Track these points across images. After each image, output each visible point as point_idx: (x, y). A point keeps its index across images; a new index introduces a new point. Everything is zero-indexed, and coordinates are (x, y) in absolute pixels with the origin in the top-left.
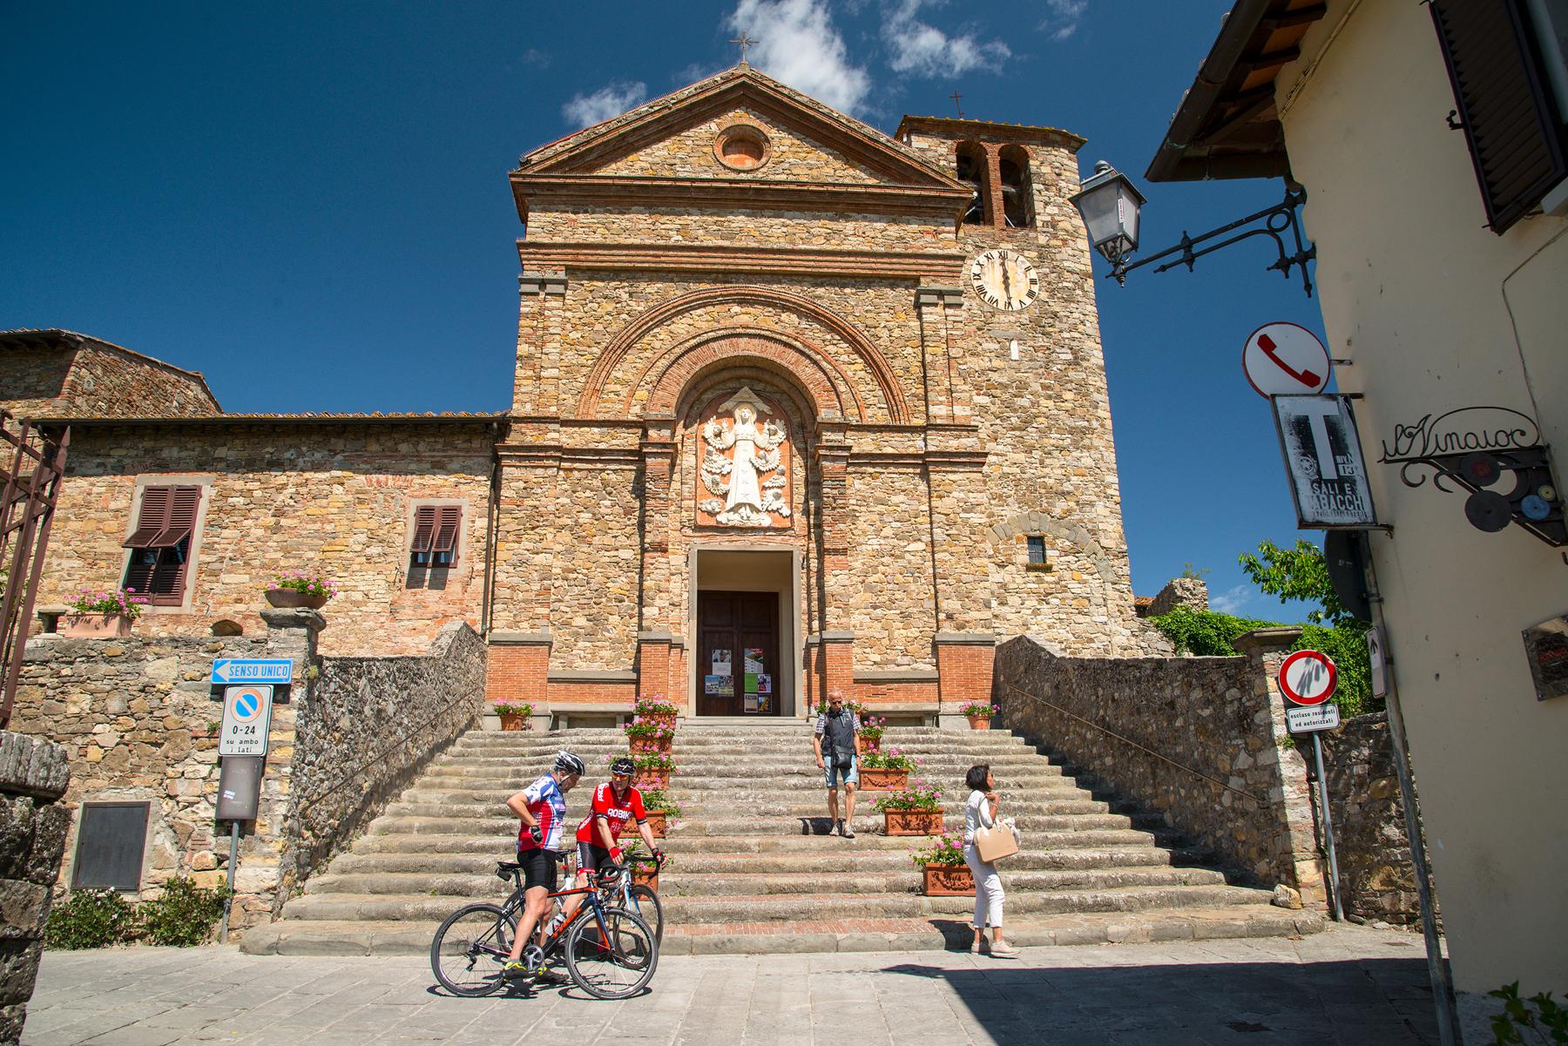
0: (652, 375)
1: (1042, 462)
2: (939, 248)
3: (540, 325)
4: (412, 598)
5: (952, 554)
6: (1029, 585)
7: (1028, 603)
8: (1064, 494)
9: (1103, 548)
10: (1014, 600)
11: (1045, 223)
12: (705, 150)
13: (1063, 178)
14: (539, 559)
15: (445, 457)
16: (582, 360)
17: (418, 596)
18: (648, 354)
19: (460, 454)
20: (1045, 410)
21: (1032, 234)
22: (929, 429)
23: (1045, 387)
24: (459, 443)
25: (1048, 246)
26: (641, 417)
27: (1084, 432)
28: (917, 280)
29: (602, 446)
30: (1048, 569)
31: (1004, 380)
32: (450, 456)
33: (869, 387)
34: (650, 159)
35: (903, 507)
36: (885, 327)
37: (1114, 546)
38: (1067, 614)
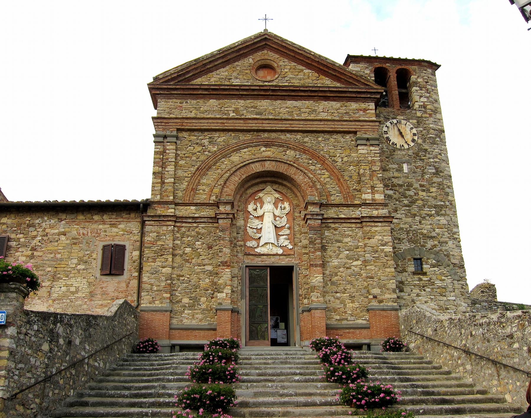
0: (221, 182)
1: (420, 222)
4: (101, 290)
5: (375, 266)
6: (415, 282)
8: (432, 237)
9: (452, 263)
10: (407, 289)
12: (247, 71)
14: (164, 270)
15: (116, 221)
17: (104, 289)
20: (421, 197)
23: (421, 186)
24: (124, 215)
25: (422, 117)
27: (441, 207)
28: (355, 133)
29: (196, 215)
30: (425, 274)
31: (400, 183)
34: (219, 76)
35: (350, 244)
37: (458, 263)
38: (434, 296)
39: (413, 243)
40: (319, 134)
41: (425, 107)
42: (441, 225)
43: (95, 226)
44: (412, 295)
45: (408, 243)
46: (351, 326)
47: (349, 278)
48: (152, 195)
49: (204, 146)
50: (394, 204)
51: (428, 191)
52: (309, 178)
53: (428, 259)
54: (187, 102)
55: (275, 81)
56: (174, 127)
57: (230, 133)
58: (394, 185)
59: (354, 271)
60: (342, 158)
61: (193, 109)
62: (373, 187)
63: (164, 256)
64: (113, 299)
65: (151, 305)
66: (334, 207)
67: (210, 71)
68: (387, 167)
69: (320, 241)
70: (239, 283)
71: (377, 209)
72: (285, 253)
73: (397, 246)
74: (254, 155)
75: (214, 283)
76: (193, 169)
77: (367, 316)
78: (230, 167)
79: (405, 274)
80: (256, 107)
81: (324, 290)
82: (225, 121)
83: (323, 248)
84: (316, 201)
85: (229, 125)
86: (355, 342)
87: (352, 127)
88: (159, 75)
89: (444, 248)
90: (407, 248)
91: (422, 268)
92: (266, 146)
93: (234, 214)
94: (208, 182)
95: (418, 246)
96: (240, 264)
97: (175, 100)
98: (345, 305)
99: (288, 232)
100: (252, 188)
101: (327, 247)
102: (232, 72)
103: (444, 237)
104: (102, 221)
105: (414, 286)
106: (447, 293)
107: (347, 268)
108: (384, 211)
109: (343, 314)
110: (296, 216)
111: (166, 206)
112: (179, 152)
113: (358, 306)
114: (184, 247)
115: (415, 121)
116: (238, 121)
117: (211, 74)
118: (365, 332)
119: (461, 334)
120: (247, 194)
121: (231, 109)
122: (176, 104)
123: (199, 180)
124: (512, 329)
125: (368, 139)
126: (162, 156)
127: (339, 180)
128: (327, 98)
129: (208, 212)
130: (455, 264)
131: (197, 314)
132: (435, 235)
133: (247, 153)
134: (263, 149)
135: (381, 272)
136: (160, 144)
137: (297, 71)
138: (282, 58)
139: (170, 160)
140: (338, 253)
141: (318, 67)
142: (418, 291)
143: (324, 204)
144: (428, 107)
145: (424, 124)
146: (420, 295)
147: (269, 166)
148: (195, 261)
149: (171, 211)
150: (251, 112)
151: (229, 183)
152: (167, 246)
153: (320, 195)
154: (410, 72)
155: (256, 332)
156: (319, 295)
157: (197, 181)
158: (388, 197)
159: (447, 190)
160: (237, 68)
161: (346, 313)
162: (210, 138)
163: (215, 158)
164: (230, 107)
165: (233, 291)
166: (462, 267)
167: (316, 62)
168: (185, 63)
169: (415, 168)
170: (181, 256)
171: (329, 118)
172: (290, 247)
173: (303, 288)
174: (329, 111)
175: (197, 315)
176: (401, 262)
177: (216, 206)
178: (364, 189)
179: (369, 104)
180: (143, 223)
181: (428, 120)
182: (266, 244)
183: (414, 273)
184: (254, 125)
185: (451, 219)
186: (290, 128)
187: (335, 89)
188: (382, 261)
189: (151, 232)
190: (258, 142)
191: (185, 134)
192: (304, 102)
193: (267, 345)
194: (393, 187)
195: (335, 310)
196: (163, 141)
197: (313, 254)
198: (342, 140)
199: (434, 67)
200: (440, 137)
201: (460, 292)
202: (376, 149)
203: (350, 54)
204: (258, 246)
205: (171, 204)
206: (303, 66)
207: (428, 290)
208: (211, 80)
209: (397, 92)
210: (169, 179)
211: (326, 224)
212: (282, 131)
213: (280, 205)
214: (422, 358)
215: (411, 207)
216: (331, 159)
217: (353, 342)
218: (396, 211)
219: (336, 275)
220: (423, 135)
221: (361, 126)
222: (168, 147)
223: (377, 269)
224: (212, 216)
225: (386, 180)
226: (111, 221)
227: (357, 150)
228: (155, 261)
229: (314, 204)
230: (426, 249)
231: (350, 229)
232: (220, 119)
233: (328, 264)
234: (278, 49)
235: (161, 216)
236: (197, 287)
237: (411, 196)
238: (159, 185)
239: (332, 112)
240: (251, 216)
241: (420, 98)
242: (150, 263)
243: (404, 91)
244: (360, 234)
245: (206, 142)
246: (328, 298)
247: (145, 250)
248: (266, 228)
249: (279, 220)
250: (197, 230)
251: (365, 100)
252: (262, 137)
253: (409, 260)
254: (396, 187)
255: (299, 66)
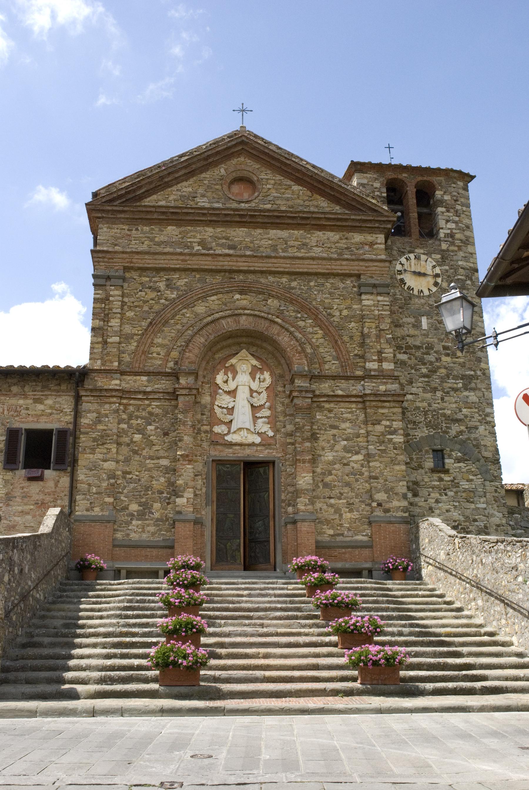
0: (181, 342)
1: (442, 399)
2: (373, 254)
3: (107, 307)
4: (21, 491)
5: (381, 462)
6: (433, 483)
7: (432, 495)
8: (458, 421)
9: (484, 457)
10: (423, 492)
11: (447, 235)
12: (217, 187)
13: (459, 203)
14: (106, 465)
15: (43, 395)
16: (135, 331)
17: (25, 490)
18: (179, 327)
19: (53, 393)
20: (444, 363)
21: (437, 243)
22: (366, 378)
23: (445, 348)
24: (52, 386)
25: (448, 250)
26: (174, 369)
27: (471, 378)
28: (358, 276)
29: (149, 389)
30: (447, 472)
31: (418, 343)
32: (46, 395)
33: (326, 349)
34: (180, 193)
35: (349, 431)
36: (337, 308)
37: (491, 456)
38: (459, 502)
39: (432, 428)
40: (310, 277)
41: (452, 235)
42: (469, 403)
43: (13, 401)
44: (430, 500)
45: (425, 429)
46: (349, 544)
47: (347, 478)
48: (90, 359)
49: (160, 291)
50: (409, 374)
51: (454, 355)
52: (297, 340)
53: (452, 450)
54: (137, 229)
55: (254, 201)
56: (120, 264)
57: (193, 273)
58: (409, 347)
59: (353, 468)
60: (341, 311)
61: (146, 239)
62: (380, 353)
63: (105, 446)
64: (38, 504)
65: (89, 513)
66: (329, 379)
67: (168, 185)
68: (401, 321)
69: (309, 427)
70: (204, 484)
71: (385, 383)
72: (264, 442)
73: (411, 432)
74: (226, 305)
75: (171, 484)
76: (144, 324)
77: (368, 531)
78: (193, 322)
79: (420, 471)
80: (227, 238)
81: (314, 494)
82: (188, 258)
83: (314, 437)
84: (305, 373)
85: (194, 263)
86: (353, 567)
87: (355, 267)
88: (100, 190)
89: (473, 436)
90: (424, 435)
91: (444, 464)
92: (241, 293)
93: (198, 389)
94: (163, 343)
95: (439, 433)
96: (205, 457)
97: (121, 226)
98: (341, 515)
99: (267, 413)
100: (221, 352)
101: (318, 436)
102: (198, 187)
103: (473, 420)
104: (24, 395)
105: (433, 488)
106: (475, 499)
107: (345, 465)
108: (393, 386)
109: (339, 528)
110: (279, 392)
111: (109, 375)
112: (126, 300)
113: (357, 517)
114: (133, 434)
115: (439, 256)
116: (204, 258)
117: (170, 189)
118: (366, 552)
119: (473, 561)
120: (214, 359)
121: (195, 240)
122: (123, 231)
123: (153, 340)
124: (516, 560)
125: (375, 286)
126: (103, 305)
127: (336, 342)
128: (322, 228)
129: (164, 384)
130: (487, 458)
131: (148, 526)
132: (462, 417)
133: (217, 302)
134: (237, 296)
135: (388, 470)
136: (101, 288)
137: (284, 187)
138: (263, 169)
139: (114, 311)
140: (333, 444)
141: (311, 184)
142: (437, 495)
143: (315, 376)
144: (458, 236)
145: (451, 260)
146: (440, 501)
147: (245, 322)
148: (147, 453)
149: (115, 383)
150: (222, 246)
151: (193, 346)
152: (109, 432)
153: (311, 363)
154: (434, 186)
155: (225, 551)
156: (308, 502)
157: (150, 340)
158: (401, 364)
159: (480, 354)
160: (205, 182)
161: (341, 525)
162: (168, 280)
163: (173, 309)
164: (195, 237)
165: (196, 495)
166: (496, 462)
167: (308, 176)
168: (136, 173)
169: (437, 322)
170: (128, 445)
171: (325, 255)
172: (271, 434)
173: (286, 491)
174: (325, 245)
175: (148, 528)
176: (416, 455)
177: (175, 376)
178: (368, 355)
179: (378, 236)
180: (78, 399)
181: (456, 255)
182: (240, 429)
183: (433, 471)
184: (226, 263)
185: (484, 395)
186: (273, 269)
187: (333, 216)
188: (389, 455)
189: (89, 411)
190: (231, 287)
191: (135, 275)
192: (292, 231)
193: (238, 570)
194: (407, 349)
195: (328, 522)
196: (104, 284)
197: (300, 446)
198: (341, 285)
199: (467, 179)
200: (471, 279)
201: (494, 496)
202: (385, 299)
203: (355, 161)
204: (229, 433)
205: (116, 373)
206: (292, 180)
207: (451, 494)
208: (170, 199)
209: (416, 215)
210: (113, 338)
211: (318, 403)
212: (262, 272)
213: (258, 376)
214: (433, 590)
215: (431, 377)
216: (326, 312)
217: (351, 567)
218: (412, 383)
219: (330, 474)
220: (449, 276)
221: (366, 267)
222: (111, 293)
223: (382, 467)
224: (169, 391)
225: (399, 339)
226: (35, 395)
227: (361, 300)
228: (93, 452)
229: (302, 376)
230: (449, 436)
231: (349, 410)
232: (181, 254)
233: (319, 458)
234: (258, 157)
235: (103, 389)
236: (147, 489)
237: (431, 363)
238: (100, 345)
239: (329, 246)
240: (220, 391)
241: (446, 224)
242: (88, 455)
243: (425, 210)
244: (362, 417)
245: (162, 285)
246: (318, 505)
247: (81, 436)
248: (240, 407)
249: (257, 397)
250: (150, 409)
251: (372, 230)
252: (236, 280)
253: (427, 452)
254: (412, 349)
255: (286, 180)
